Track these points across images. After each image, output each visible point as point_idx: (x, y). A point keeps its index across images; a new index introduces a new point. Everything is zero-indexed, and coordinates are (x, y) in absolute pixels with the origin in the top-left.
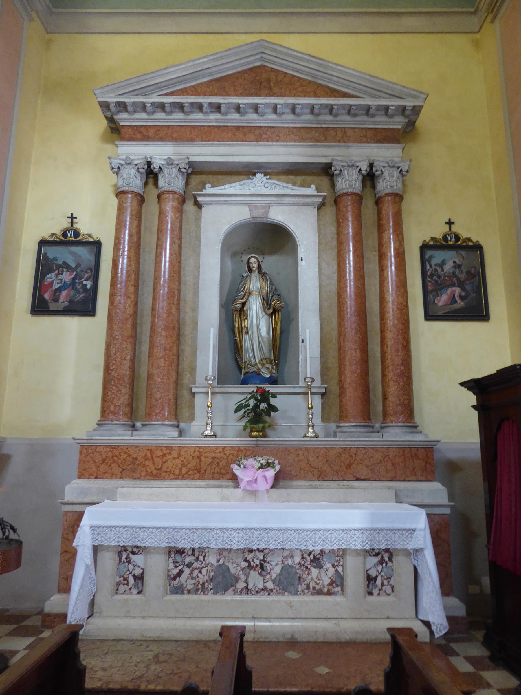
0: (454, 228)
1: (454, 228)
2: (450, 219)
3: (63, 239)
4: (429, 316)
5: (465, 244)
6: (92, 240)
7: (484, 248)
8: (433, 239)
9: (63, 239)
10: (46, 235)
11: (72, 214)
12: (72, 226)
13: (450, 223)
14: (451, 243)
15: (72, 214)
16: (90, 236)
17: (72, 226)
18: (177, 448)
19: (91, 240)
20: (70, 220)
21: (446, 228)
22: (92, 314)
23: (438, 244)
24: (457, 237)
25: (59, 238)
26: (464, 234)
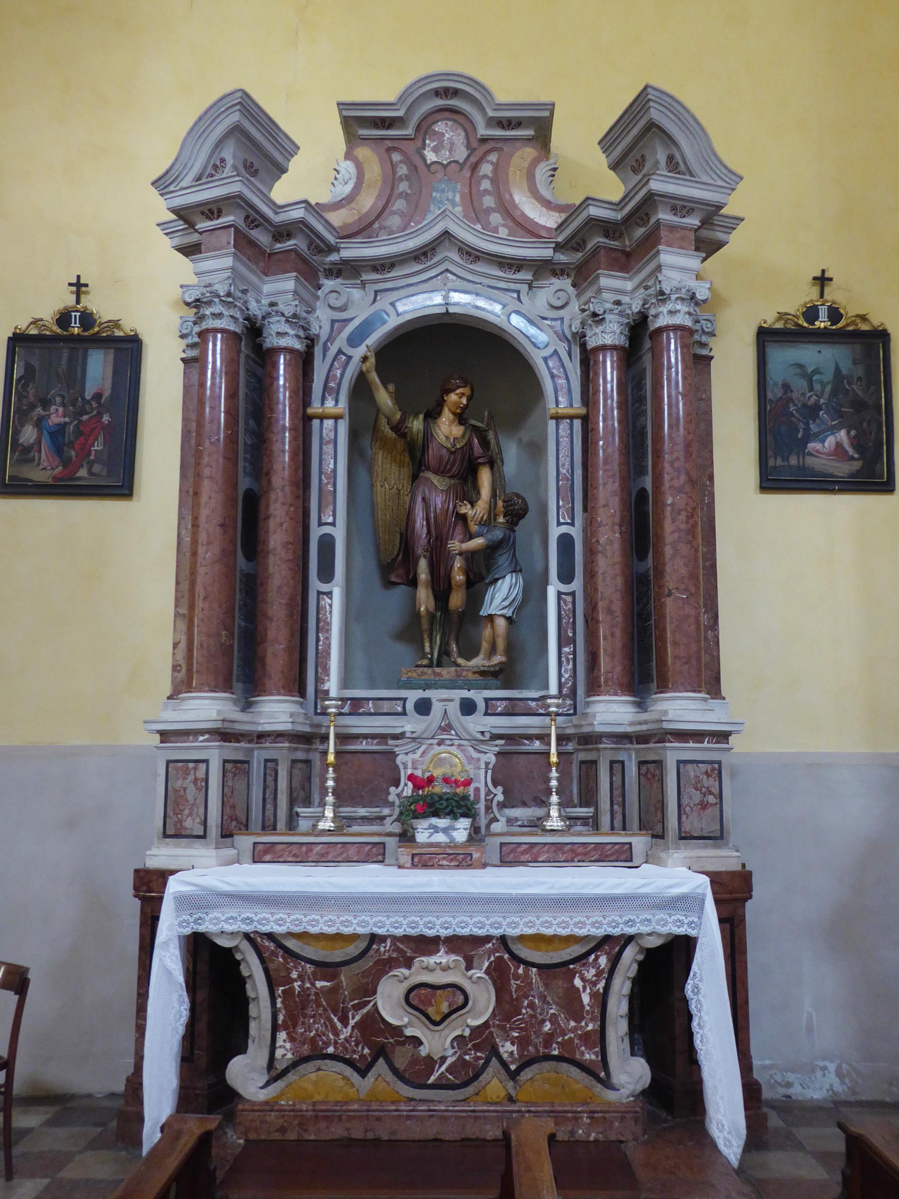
0: (832, 294)
1: (832, 294)
2: (823, 271)
3: (59, 331)
4: (772, 480)
5: (851, 328)
6: (121, 334)
7: (892, 336)
8: (781, 316)
9: (59, 331)
10: (769, 318)
11: (78, 277)
12: (78, 301)
13: (822, 280)
14: (76, 331)
15: (78, 277)
16: (863, 318)
17: (78, 301)
18: (215, 754)
19: (864, 327)
20: (74, 289)
21: (813, 294)
22: (127, 492)
23: (48, 333)
24: (835, 314)
25: (51, 331)
26: (851, 309)
